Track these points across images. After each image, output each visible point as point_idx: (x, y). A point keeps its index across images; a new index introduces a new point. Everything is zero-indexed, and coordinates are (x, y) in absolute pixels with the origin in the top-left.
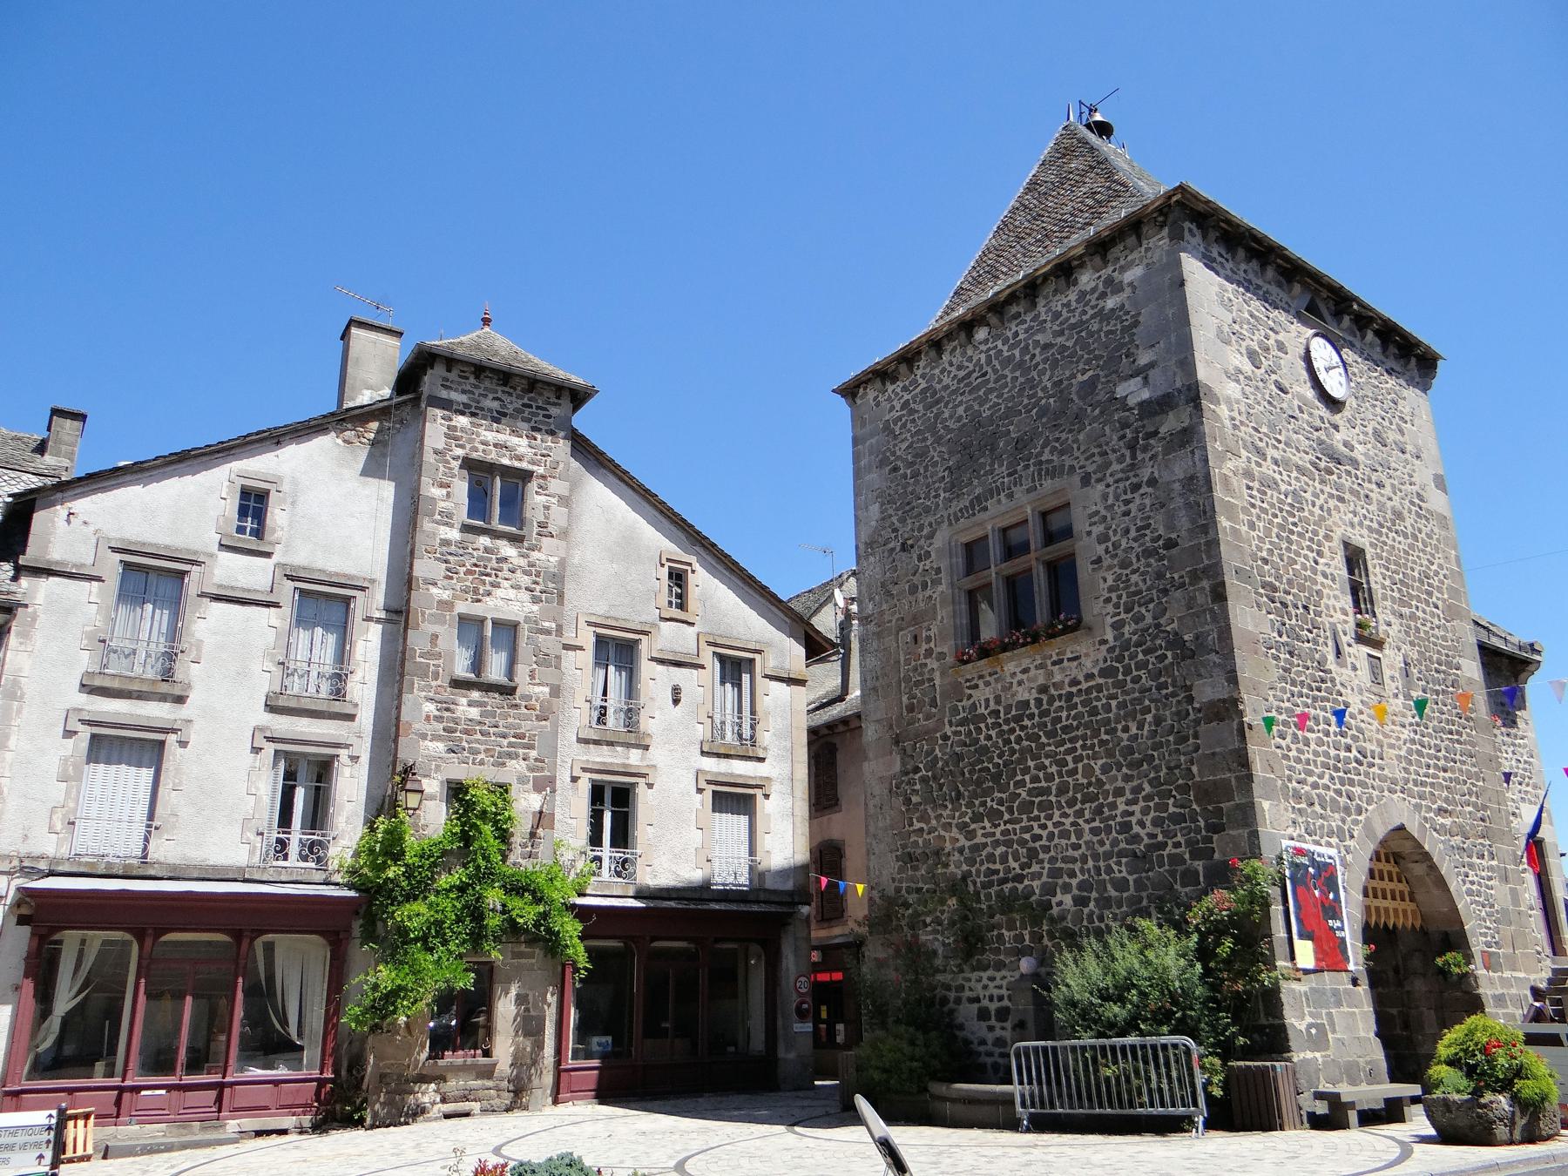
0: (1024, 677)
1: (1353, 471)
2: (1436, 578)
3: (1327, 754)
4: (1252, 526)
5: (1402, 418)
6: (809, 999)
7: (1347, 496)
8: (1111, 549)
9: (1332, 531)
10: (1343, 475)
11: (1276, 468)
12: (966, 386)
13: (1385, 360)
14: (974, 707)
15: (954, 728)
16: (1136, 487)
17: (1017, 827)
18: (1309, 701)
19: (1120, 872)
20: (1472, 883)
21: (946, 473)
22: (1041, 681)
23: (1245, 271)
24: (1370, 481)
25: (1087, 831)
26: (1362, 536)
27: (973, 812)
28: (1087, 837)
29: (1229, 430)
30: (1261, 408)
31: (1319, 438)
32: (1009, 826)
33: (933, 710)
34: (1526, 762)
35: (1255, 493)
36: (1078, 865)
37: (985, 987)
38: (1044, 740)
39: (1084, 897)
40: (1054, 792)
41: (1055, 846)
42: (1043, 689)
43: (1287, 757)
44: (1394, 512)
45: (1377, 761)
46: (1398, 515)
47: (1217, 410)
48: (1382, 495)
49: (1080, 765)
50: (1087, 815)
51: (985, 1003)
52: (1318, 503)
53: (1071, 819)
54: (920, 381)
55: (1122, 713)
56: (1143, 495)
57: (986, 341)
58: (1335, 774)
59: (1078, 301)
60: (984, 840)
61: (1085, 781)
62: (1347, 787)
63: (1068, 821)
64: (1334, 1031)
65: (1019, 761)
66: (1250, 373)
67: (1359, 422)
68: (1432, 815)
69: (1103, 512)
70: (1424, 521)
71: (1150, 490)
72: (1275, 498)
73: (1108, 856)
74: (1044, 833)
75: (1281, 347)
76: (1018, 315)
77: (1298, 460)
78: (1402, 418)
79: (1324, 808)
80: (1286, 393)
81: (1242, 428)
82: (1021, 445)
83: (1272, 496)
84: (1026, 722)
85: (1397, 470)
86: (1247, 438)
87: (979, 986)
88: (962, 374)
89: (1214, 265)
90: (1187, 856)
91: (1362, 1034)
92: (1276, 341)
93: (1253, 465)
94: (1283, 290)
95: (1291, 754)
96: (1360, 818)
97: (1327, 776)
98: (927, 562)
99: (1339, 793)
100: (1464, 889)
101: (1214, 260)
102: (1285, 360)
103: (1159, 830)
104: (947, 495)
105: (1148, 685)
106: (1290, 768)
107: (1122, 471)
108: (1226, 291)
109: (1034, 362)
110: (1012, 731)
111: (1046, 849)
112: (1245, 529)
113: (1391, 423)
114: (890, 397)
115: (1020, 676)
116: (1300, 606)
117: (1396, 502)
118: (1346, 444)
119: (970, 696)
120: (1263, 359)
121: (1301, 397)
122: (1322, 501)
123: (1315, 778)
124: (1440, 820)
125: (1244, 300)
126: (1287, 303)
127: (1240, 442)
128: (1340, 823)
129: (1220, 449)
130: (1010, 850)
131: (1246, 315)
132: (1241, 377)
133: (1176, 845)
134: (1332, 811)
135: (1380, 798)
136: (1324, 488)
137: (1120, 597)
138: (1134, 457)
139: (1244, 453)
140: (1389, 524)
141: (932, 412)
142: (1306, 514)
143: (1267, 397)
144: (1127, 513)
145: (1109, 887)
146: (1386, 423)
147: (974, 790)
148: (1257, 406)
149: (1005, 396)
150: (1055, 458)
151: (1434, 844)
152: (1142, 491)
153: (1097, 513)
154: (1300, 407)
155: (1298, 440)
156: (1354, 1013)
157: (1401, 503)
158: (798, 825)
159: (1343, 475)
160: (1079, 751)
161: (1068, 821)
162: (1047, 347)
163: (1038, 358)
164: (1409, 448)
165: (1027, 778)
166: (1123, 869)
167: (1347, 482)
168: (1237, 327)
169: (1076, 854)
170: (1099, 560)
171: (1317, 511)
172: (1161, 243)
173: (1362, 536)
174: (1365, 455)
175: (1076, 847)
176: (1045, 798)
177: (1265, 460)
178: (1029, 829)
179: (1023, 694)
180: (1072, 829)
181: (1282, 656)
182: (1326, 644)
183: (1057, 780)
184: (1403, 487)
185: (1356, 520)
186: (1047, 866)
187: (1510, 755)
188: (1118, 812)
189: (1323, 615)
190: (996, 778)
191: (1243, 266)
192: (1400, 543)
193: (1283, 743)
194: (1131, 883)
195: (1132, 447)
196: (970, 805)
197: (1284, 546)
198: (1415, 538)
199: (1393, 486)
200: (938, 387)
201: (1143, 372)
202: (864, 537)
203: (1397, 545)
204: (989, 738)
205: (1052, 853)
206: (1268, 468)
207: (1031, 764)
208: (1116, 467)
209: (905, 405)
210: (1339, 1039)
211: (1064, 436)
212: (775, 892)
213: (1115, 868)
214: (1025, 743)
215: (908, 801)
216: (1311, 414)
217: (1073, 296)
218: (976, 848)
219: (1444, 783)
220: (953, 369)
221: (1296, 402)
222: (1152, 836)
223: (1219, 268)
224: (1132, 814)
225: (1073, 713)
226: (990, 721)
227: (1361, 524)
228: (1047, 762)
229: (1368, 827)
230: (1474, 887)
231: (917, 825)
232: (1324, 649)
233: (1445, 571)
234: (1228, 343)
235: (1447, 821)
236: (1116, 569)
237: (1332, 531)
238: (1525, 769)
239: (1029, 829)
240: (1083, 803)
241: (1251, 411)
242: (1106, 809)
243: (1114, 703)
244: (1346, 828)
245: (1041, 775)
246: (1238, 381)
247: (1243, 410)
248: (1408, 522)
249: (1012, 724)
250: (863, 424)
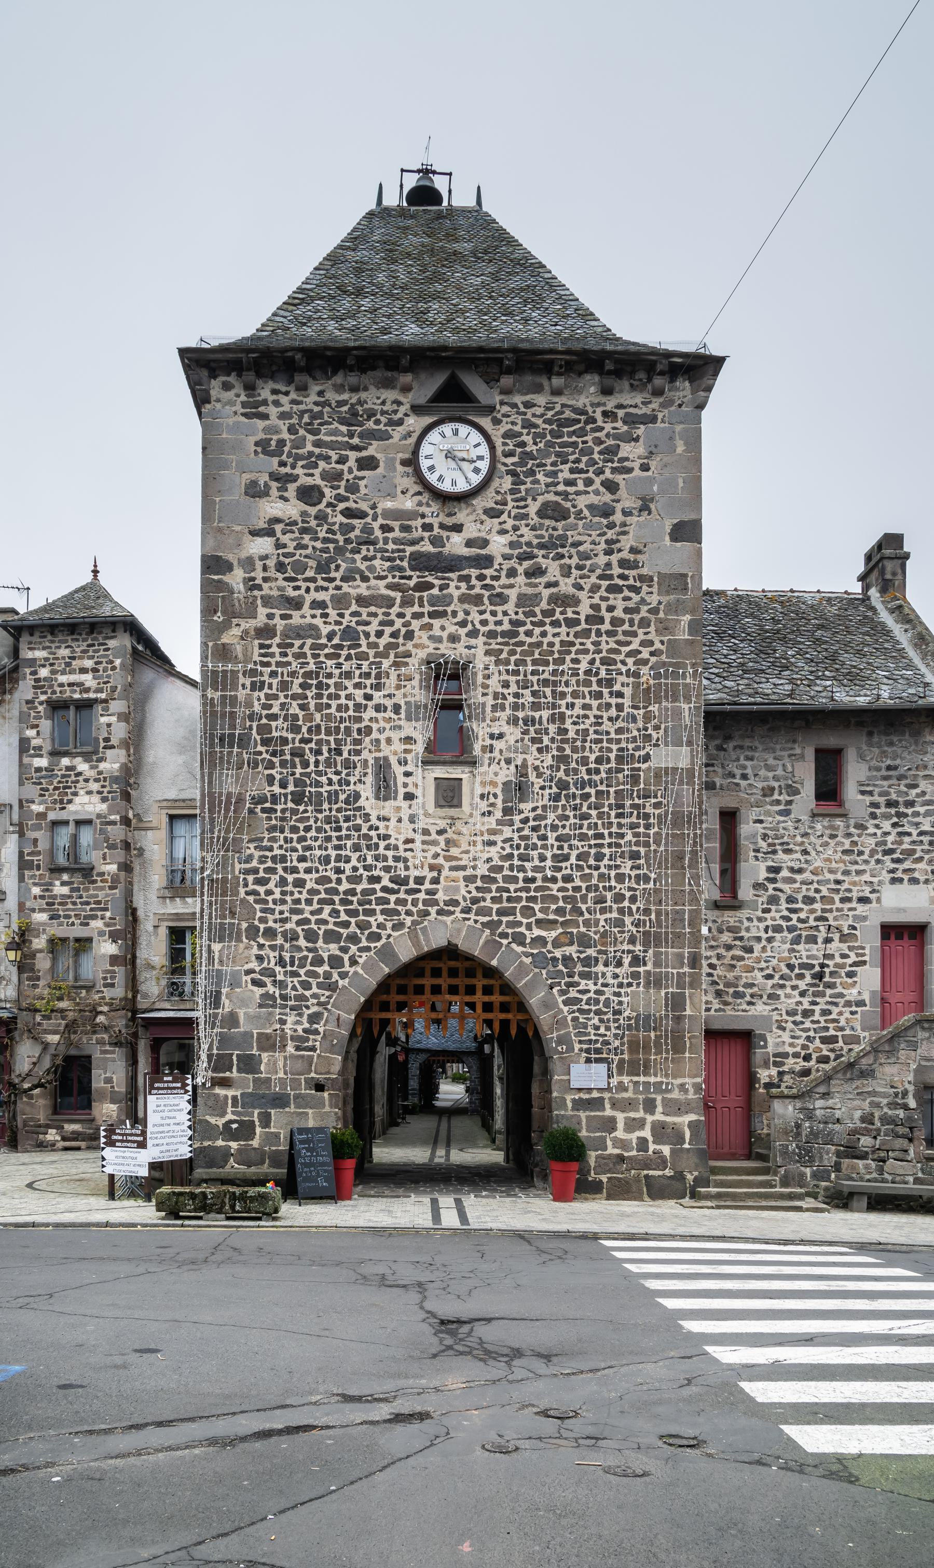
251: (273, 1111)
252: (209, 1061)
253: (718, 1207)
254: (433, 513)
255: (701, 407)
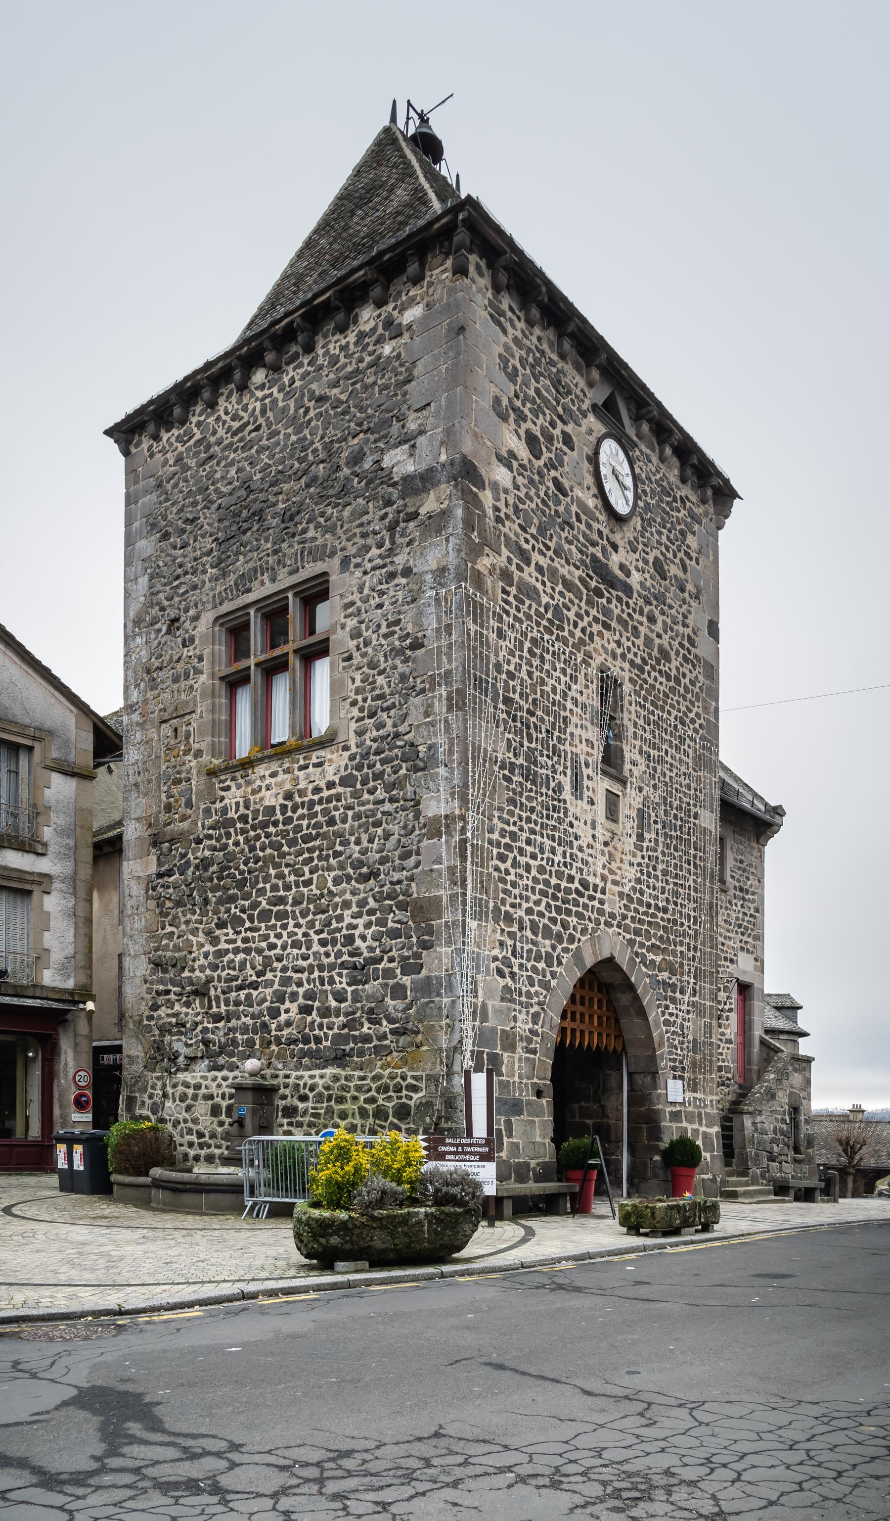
0: (273, 780)
1: (625, 599)
2: (692, 726)
3: (547, 883)
4: (501, 634)
5: (687, 554)
6: (89, 1093)
7: (614, 624)
8: (362, 646)
9: (591, 658)
10: (614, 601)
11: (540, 577)
12: (240, 441)
13: (681, 486)
14: (225, 810)
15: (205, 831)
16: (392, 576)
17: (256, 934)
18: (538, 828)
19: (341, 983)
20: (671, 1015)
21: (214, 545)
22: (288, 787)
23: (539, 339)
24: (641, 613)
25: (316, 942)
26: (622, 669)
27: (219, 918)
28: (316, 947)
29: (490, 522)
30: (533, 506)
31: (593, 555)
32: (249, 934)
33: (189, 811)
34: (751, 916)
35: (511, 599)
36: (305, 976)
37: (219, 1086)
38: (285, 848)
39: (308, 1005)
40: (290, 901)
41: (288, 955)
42: (288, 796)
43: (503, 880)
44: (661, 649)
45: (598, 895)
46: (664, 655)
47: (480, 494)
48: (652, 631)
49: (315, 876)
50: (318, 926)
51: (218, 1100)
52: (581, 625)
53: (303, 929)
54: (195, 430)
55: (356, 823)
56: (397, 585)
57: (262, 387)
58: (552, 903)
59: (356, 344)
60: (226, 946)
61: (318, 892)
62: (563, 916)
63: (300, 932)
64: (510, 1135)
65: (261, 870)
66: (526, 462)
67: (641, 547)
68: (644, 951)
69: (359, 604)
70: (690, 666)
71: (404, 581)
72: (533, 610)
73: (332, 967)
74: (279, 943)
75: (567, 440)
76: (296, 356)
77: (566, 573)
78: (687, 554)
79: (535, 933)
80: (565, 495)
81: (507, 523)
82: (288, 517)
83: (530, 607)
84: (272, 829)
85: (671, 607)
86: (512, 535)
87: (214, 1084)
88: (236, 425)
89: (502, 319)
90: (398, 971)
91: (538, 1139)
92: (563, 432)
93: (513, 568)
94: (582, 375)
95: (508, 878)
96: (571, 947)
97: (544, 904)
98: (191, 648)
99: (553, 921)
100: (662, 1019)
101: (502, 314)
102: (570, 457)
103: (377, 943)
104: (214, 570)
105: (382, 797)
106: (505, 891)
107: (380, 556)
108: (513, 356)
109: (307, 418)
110: (258, 837)
111: (279, 959)
112: (493, 636)
113: (675, 556)
114: (164, 447)
115: (268, 780)
116: (543, 730)
117: (665, 640)
118: (622, 567)
119: (222, 799)
120: (544, 449)
121: (581, 505)
122: (585, 623)
123: (531, 904)
124: (650, 956)
125: (533, 374)
126: (582, 391)
127: (502, 538)
128: (550, 950)
129: (477, 540)
130: (248, 958)
131: (532, 392)
132: (515, 464)
133: (391, 960)
134: (543, 938)
135: (594, 931)
136: (590, 610)
137: (365, 700)
138: (393, 542)
139: (504, 551)
140: (654, 663)
141: (204, 470)
142: (566, 634)
143: (542, 494)
144: (380, 606)
145: (330, 997)
146: (670, 555)
147: (221, 897)
148: (528, 502)
149: (277, 456)
150: (318, 535)
151: (640, 978)
152: (396, 581)
153: (353, 603)
154: (577, 514)
155: (569, 550)
156: (534, 1121)
157: (670, 643)
158: (81, 925)
159: (614, 601)
160: (316, 862)
161: (300, 932)
162: (321, 399)
163: (312, 414)
164: (690, 587)
165: (268, 886)
166: (344, 980)
167: (616, 609)
168: (518, 404)
169: (305, 964)
170: (349, 658)
171: (578, 633)
172: (444, 276)
173: (622, 669)
174: (641, 583)
175: (305, 958)
176: (282, 907)
177: (528, 565)
178: (266, 938)
179: (270, 799)
180: (303, 939)
181: (515, 779)
182: (565, 774)
183: (294, 890)
184: (675, 627)
185: (619, 651)
186: (279, 974)
187: (739, 908)
188: (344, 924)
189: (567, 743)
190: (241, 884)
191: (537, 331)
192: (661, 683)
193: (502, 866)
194: (349, 994)
195: (392, 528)
196: (216, 912)
197: (535, 664)
198: (678, 682)
199: (664, 622)
200: (213, 439)
201: (409, 439)
202: (132, 614)
203: (657, 685)
204: (237, 844)
205: (285, 962)
206: (529, 575)
207: (272, 872)
208: (375, 551)
209: (179, 460)
210: (514, 1143)
211: (329, 510)
212: (54, 989)
213: (337, 979)
214: (268, 851)
215: (160, 905)
216: (589, 526)
217: (352, 338)
218: (220, 954)
219: (662, 923)
220: (227, 418)
221: (574, 508)
222: (371, 949)
223: (508, 325)
224: (355, 927)
225: (313, 822)
226: (239, 825)
227: (623, 656)
228: (286, 871)
229: (578, 956)
230: (672, 1019)
231: (169, 929)
232: (562, 778)
233: (702, 721)
234: (504, 418)
235: (659, 959)
236: (365, 669)
237: (591, 658)
238: (749, 922)
239: (266, 938)
240: (314, 914)
241: (521, 506)
242: (334, 921)
243: (350, 813)
244: (555, 955)
245: (280, 883)
246: (510, 468)
247: (511, 502)
248: (674, 664)
249: (259, 831)
250: (136, 482)
251: (513, 1119)
252: (472, 1056)
253: (758, 1202)
254: (602, 522)
255: (720, 528)
